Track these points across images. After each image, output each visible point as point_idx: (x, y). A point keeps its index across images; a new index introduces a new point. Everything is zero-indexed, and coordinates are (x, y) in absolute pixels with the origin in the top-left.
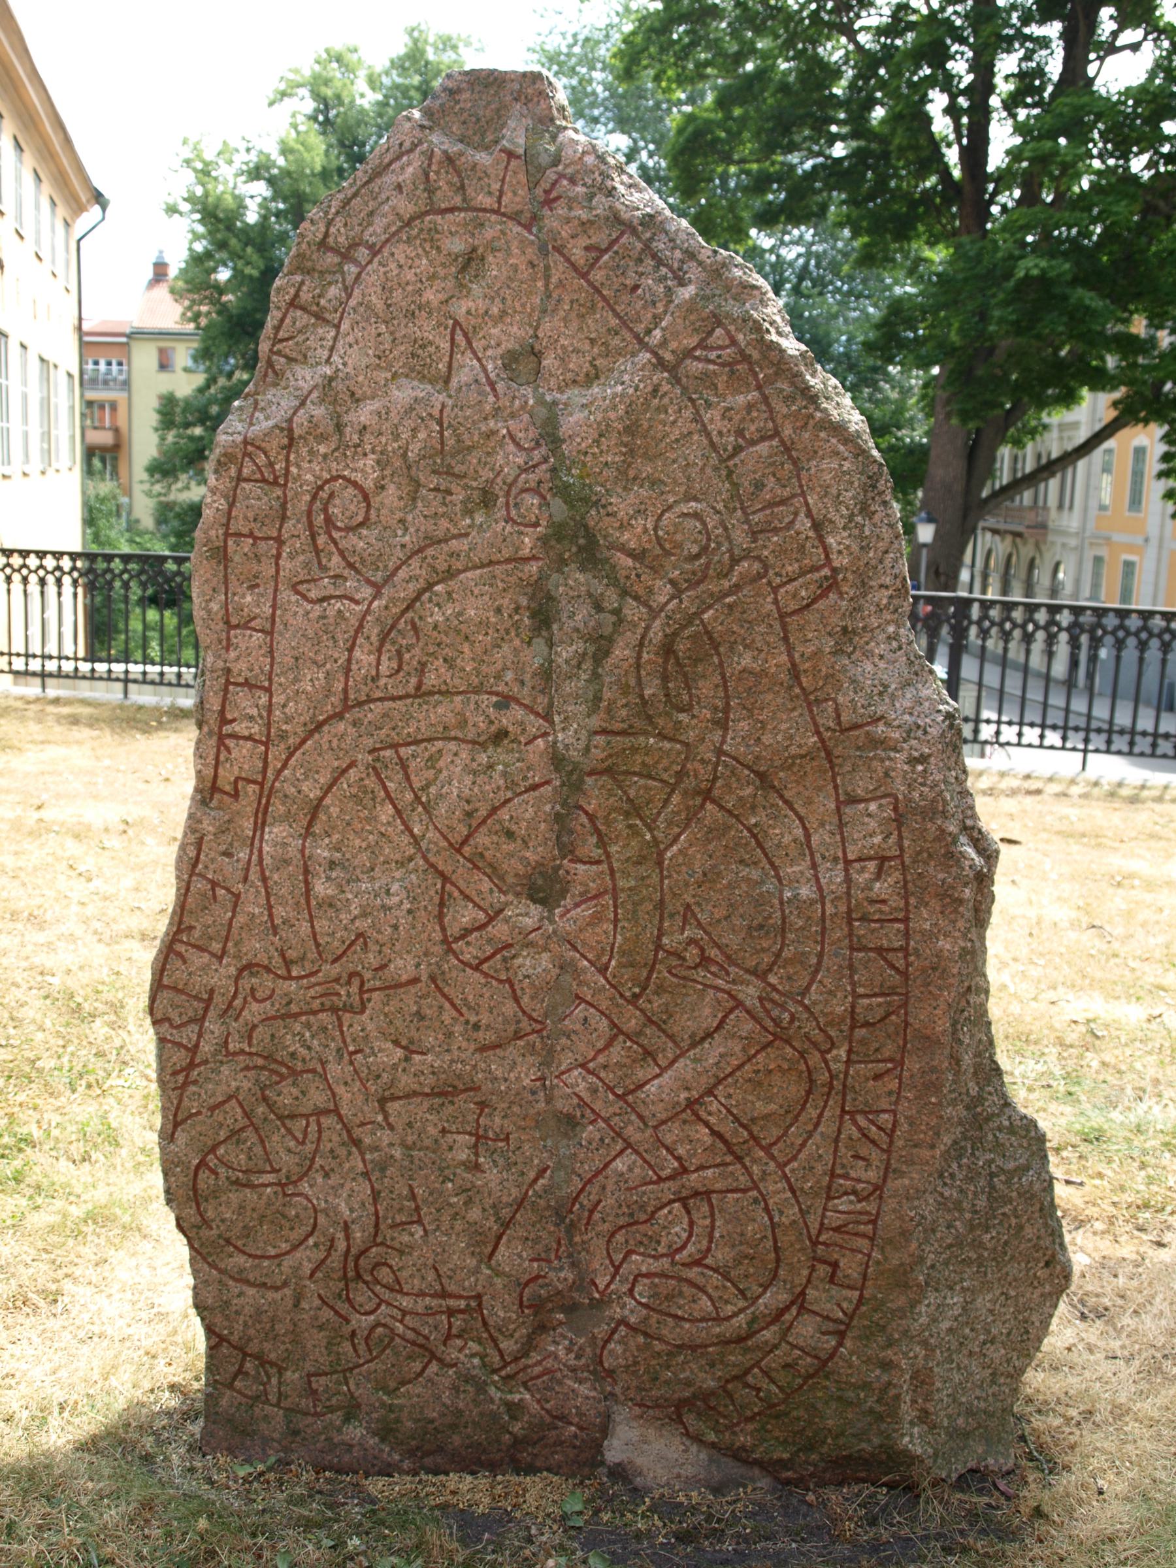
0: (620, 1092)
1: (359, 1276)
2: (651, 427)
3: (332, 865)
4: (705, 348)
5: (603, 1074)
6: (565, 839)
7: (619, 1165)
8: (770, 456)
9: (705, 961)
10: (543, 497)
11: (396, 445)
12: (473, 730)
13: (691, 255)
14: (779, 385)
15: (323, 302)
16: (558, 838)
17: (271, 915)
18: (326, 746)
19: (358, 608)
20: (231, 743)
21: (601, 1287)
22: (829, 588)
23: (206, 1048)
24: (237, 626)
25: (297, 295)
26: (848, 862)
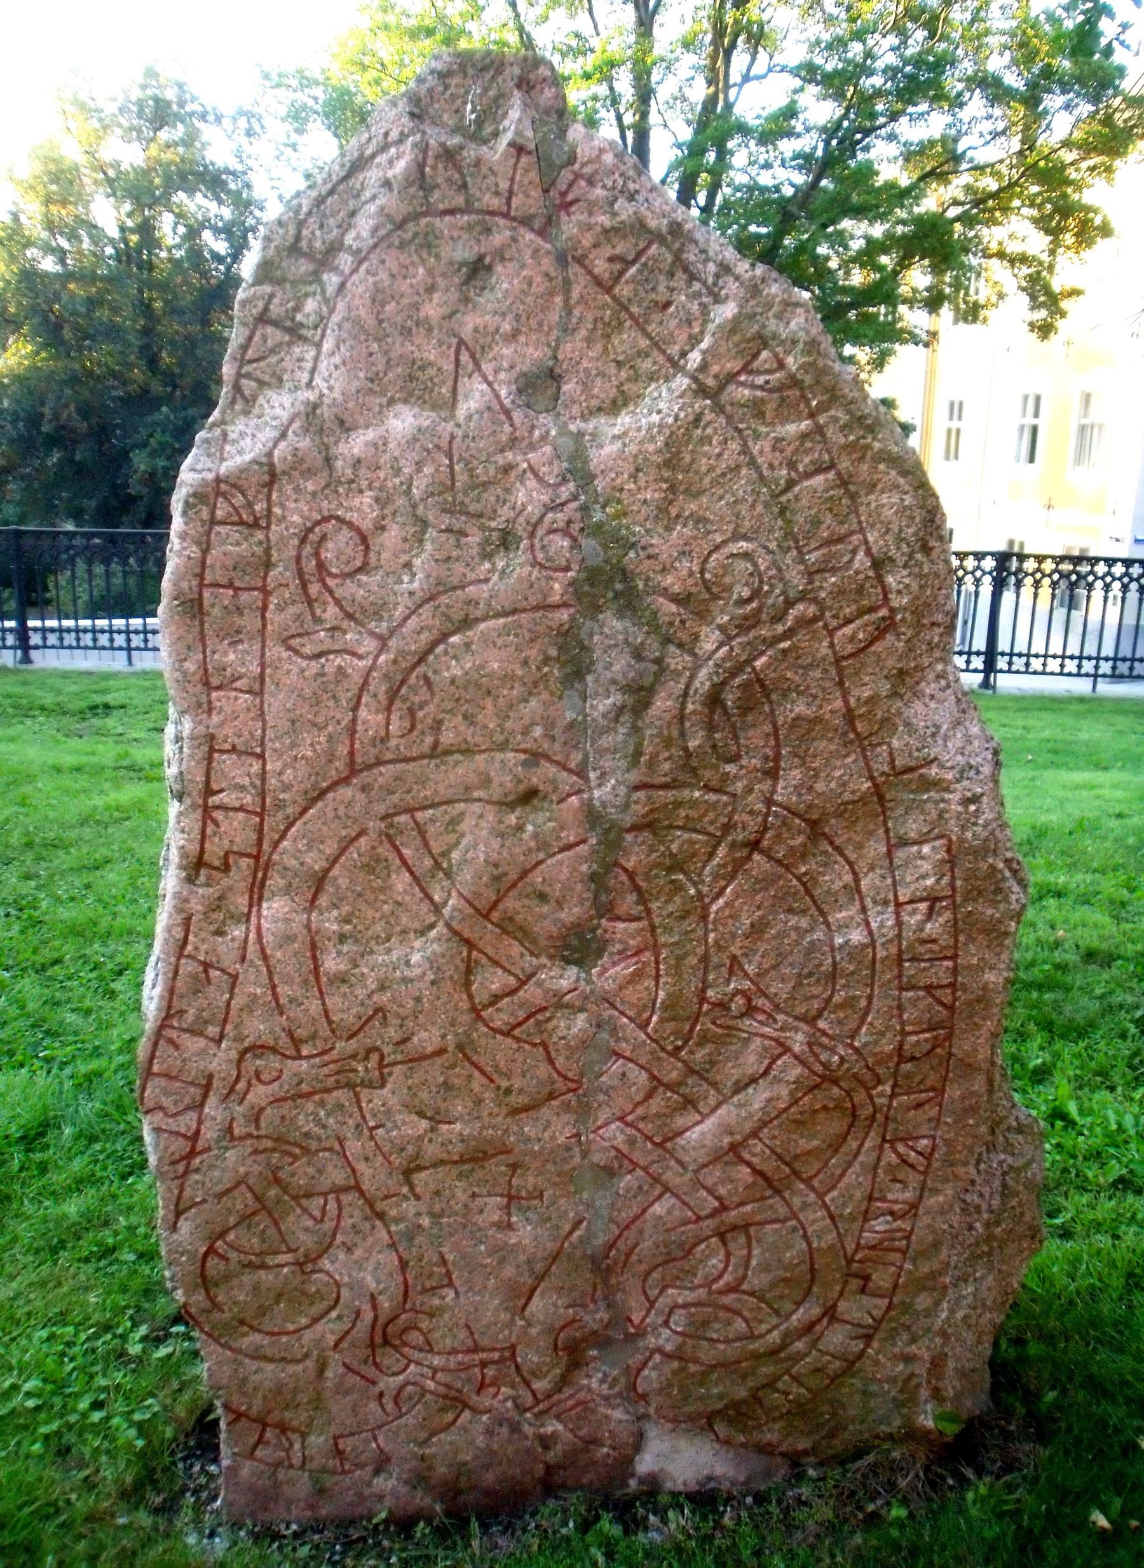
0: (657, 1140)
1: (386, 1342)
2: (693, 461)
3: (342, 938)
4: (751, 372)
5: (641, 1125)
6: (603, 898)
7: (658, 1209)
8: (827, 490)
11: (397, 481)
13: (725, 269)
19: (362, 664)
20: (218, 815)
21: (637, 1321)
23: (209, 1133)
24: (219, 688)
25: (266, 309)
26: (898, 905)
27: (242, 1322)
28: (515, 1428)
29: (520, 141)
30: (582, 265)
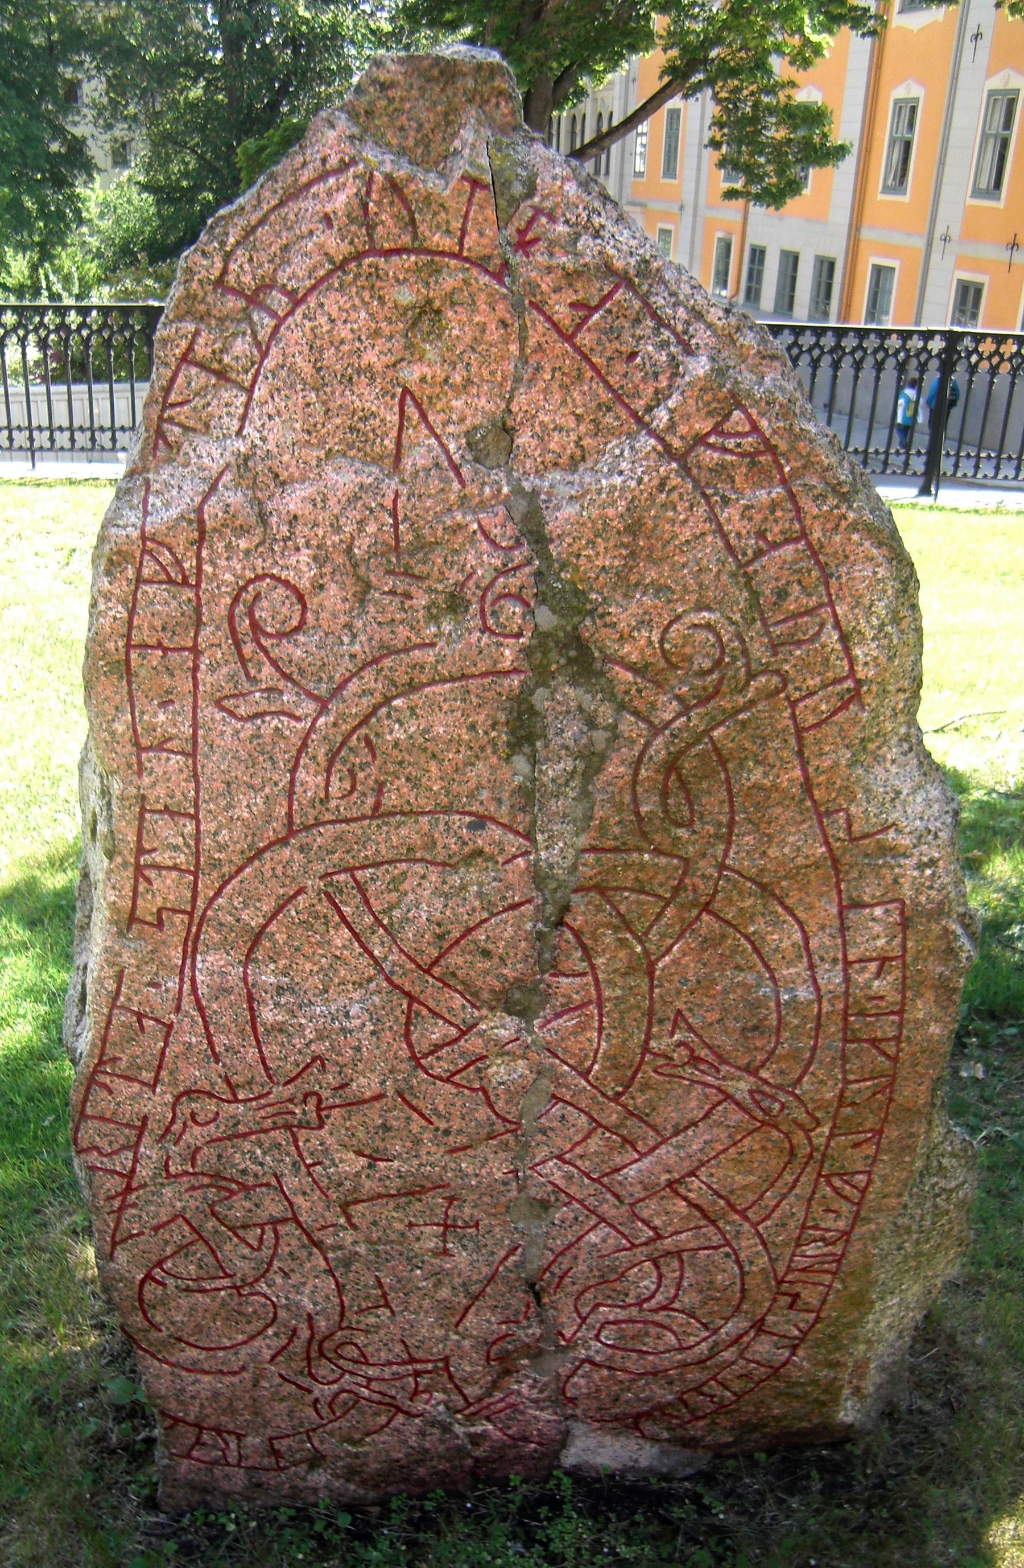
1: (322, 1354)
4: (721, 434)
5: (579, 1163)
7: (593, 1237)
8: (795, 562)
9: (695, 1060)
10: (527, 604)
11: (336, 539)
12: (443, 852)
14: (807, 480)
15: (227, 359)
16: (540, 955)
17: (211, 1044)
18: (268, 874)
19: (299, 726)
20: (152, 874)
21: (568, 1335)
22: (850, 701)
23: (144, 1172)
24: (147, 749)
25: (190, 348)
26: (847, 964)
27: (179, 1340)
28: (446, 1428)
29: (473, 172)
30: (543, 313)
